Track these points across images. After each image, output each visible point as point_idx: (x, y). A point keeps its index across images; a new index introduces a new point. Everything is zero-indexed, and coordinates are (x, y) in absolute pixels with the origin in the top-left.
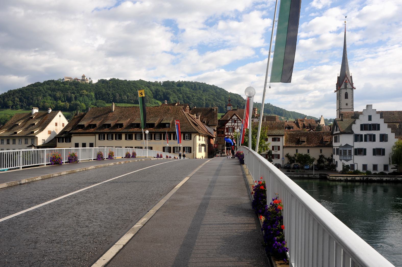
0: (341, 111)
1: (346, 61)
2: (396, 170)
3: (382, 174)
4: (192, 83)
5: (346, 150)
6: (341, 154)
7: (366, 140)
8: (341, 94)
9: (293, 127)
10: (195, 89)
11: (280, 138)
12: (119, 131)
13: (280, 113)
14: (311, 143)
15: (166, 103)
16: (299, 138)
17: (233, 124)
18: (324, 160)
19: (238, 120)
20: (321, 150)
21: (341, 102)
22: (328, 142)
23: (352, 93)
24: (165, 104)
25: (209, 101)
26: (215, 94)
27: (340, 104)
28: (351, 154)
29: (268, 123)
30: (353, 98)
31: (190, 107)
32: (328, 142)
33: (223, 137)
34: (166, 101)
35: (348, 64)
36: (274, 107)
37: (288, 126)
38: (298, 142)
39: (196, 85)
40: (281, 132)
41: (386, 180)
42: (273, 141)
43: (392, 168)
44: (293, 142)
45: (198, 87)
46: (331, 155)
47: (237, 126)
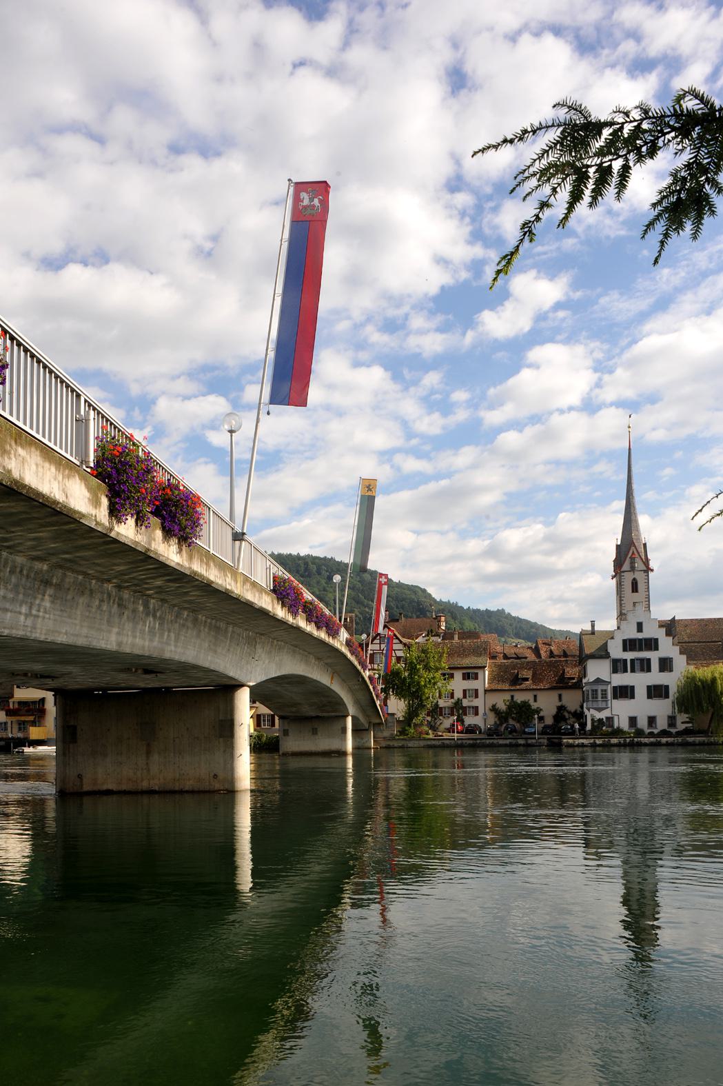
1: (632, 511)
2: (690, 725)
3: (664, 733)
4: (298, 557)
5: (596, 690)
7: (633, 671)
10: (307, 573)
13: (532, 634)
14: (541, 681)
16: (518, 672)
18: (566, 715)
20: (560, 696)
22: (573, 678)
23: (646, 581)
27: (621, 605)
28: (606, 697)
30: (648, 591)
32: (573, 678)
36: (514, 618)
38: (516, 681)
39: (310, 563)
40: (479, 661)
41: (667, 742)
42: (464, 679)
43: (682, 723)
45: (313, 568)
46: (580, 704)
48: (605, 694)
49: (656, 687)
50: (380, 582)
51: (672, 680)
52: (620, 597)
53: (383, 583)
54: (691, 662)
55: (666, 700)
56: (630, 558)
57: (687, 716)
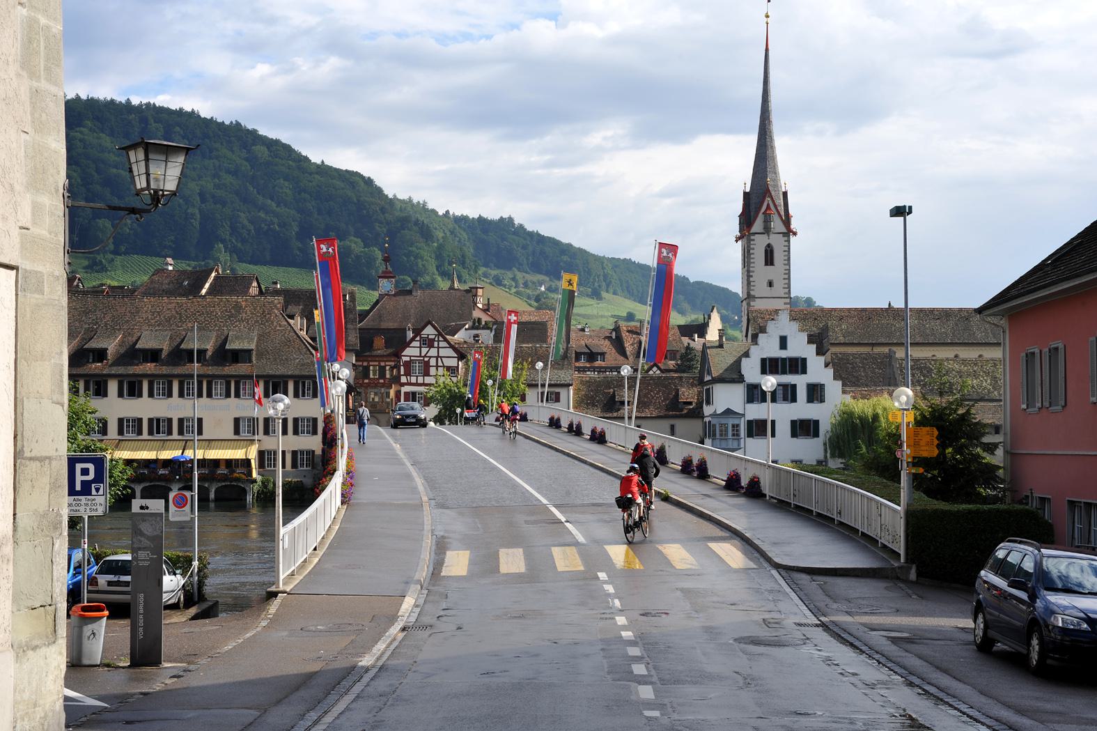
0: (752, 304)
1: (768, 143)
6: (714, 435)
7: (774, 400)
8: (753, 249)
9: (603, 354)
11: (559, 393)
12: (97, 372)
15: (170, 268)
17: (424, 350)
19: (438, 338)
21: (752, 276)
23: (786, 249)
24: (167, 270)
25: (218, 206)
26: (246, 166)
27: (749, 283)
28: (738, 435)
29: (525, 349)
31: (259, 287)
32: (690, 403)
33: (366, 387)
34: (171, 259)
35: (773, 152)
37: (587, 351)
44: (597, 406)
47: (437, 358)
48: (737, 430)
49: (802, 421)
50: (509, 320)
51: (825, 414)
52: (748, 271)
53: (512, 321)
54: (847, 389)
55: (816, 439)
56: (762, 209)
57: (840, 460)
